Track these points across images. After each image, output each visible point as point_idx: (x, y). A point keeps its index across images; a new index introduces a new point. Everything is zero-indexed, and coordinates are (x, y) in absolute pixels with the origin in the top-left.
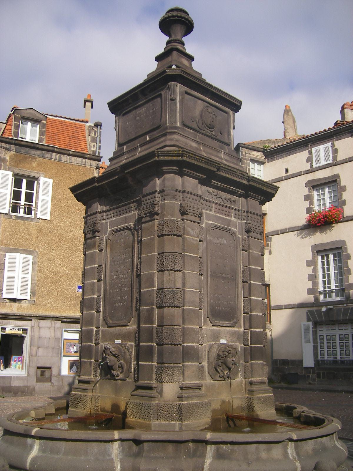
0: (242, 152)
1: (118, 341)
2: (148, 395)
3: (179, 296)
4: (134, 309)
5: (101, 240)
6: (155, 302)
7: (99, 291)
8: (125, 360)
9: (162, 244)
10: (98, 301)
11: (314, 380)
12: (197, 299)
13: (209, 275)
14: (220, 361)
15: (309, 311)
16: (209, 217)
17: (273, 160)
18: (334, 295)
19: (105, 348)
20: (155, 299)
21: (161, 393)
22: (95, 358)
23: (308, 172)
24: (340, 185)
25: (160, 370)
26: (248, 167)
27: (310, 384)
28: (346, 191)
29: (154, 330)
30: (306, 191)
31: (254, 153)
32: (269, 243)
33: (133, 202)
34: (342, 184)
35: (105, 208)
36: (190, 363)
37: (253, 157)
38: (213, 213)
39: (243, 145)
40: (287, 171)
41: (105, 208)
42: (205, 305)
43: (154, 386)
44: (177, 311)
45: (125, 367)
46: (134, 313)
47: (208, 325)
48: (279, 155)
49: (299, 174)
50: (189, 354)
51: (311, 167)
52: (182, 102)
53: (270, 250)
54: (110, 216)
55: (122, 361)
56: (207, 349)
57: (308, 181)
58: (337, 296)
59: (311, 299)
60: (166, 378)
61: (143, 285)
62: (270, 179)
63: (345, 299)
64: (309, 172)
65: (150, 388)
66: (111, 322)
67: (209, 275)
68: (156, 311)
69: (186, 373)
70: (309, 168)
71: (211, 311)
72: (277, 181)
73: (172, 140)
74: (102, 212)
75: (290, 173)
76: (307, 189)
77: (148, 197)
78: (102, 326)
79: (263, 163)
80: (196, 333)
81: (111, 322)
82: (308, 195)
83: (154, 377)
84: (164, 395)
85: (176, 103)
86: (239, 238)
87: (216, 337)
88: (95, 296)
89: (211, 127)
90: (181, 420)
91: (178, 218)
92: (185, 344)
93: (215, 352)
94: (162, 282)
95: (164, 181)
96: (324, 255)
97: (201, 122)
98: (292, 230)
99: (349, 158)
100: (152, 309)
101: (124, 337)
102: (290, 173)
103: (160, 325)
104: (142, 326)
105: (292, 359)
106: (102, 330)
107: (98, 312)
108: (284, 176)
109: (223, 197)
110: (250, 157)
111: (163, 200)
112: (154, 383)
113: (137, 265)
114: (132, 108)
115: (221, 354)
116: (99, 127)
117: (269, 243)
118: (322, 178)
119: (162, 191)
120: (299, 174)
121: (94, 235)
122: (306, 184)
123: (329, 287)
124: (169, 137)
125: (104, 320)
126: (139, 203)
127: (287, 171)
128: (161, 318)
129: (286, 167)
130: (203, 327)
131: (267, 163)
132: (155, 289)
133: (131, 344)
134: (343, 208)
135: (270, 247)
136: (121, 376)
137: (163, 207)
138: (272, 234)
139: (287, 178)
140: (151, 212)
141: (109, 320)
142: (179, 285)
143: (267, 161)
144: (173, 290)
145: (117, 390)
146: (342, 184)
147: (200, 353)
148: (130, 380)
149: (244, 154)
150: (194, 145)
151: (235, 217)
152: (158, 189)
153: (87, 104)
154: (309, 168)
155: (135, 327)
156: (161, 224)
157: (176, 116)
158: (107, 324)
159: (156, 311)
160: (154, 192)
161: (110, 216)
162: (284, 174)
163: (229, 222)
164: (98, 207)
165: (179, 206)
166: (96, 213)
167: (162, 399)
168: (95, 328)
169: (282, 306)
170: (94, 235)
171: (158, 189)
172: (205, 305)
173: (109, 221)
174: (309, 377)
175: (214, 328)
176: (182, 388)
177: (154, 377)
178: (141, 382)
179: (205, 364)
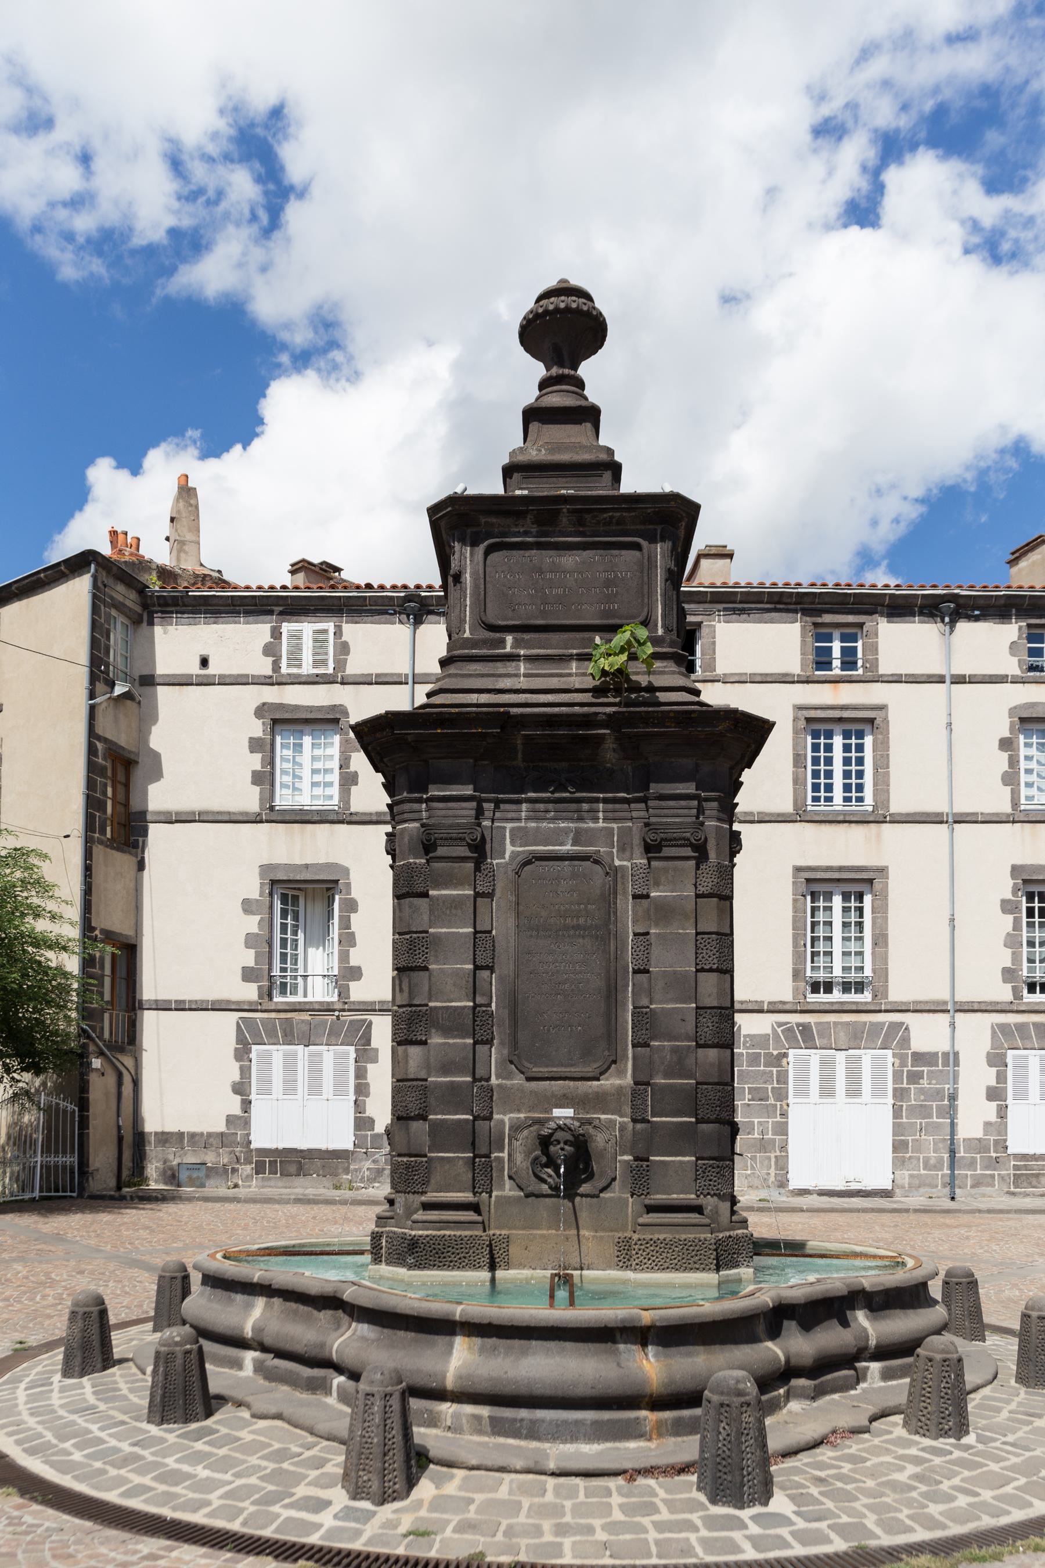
11: (249, 1178)
30: (258, 729)
32: (141, 839)
40: (204, 662)
57: (264, 704)
59: (250, 992)
72: (176, 681)
75: (213, 670)
102: (213, 670)
108: (197, 676)
117: (141, 839)
127: (204, 662)
129: (204, 653)
162: (195, 669)
175: (534, 1084)
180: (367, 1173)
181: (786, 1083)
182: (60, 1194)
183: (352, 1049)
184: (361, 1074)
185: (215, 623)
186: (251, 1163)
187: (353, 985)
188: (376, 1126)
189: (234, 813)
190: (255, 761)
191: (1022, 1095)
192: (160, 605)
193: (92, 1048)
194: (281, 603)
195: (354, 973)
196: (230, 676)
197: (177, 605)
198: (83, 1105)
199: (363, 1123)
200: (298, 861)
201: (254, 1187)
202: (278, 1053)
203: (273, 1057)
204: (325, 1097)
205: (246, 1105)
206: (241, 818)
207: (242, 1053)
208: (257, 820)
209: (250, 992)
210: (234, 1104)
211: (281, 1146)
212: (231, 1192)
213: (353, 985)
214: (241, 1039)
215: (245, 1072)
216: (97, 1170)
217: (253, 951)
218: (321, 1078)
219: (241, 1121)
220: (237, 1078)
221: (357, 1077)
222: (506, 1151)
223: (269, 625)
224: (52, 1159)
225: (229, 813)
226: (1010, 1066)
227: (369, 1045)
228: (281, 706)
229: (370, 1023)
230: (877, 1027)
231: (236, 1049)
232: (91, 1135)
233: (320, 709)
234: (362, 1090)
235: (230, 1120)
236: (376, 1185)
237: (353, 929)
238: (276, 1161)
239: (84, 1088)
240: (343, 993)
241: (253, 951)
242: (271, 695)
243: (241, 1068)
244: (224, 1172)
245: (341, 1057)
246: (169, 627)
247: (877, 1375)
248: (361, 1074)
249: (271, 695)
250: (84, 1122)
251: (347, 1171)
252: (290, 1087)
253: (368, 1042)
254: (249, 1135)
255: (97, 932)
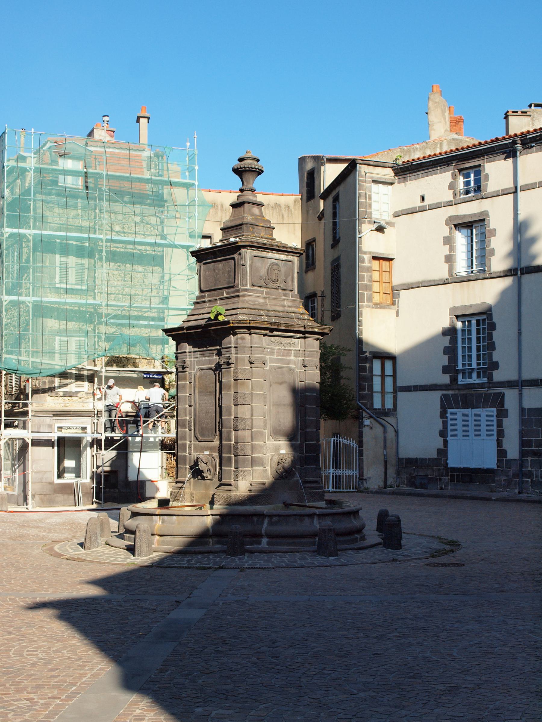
0: (360, 171)
1: (207, 453)
2: (229, 489)
3: (248, 422)
4: (218, 430)
5: (190, 374)
6: (232, 427)
7: (190, 414)
8: (212, 465)
9: (236, 385)
10: (190, 422)
11: (446, 484)
12: (262, 424)
13: (271, 405)
14: (279, 466)
15: (443, 395)
16: (271, 361)
17: (405, 179)
18: (474, 375)
19: (197, 458)
20: (232, 425)
21: (237, 488)
22: (189, 464)
23: (449, 204)
24: (489, 227)
25: (236, 472)
26: (368, 193)
27: (441, 489)
28: (495, 236)
29: (232, 446)
30: (445, 231)
31: (379, 170)
32: (397, 300)
33: (215, 350)
34: (492, 226)
35: (192, 350)
36: (257, 468)
37: (376, 177)
38: (275, 357)
39: (361, 162)
40: (423, 198)
41: (192, 350)
42: (268, 426)
43: (232, 483)
44: (247, 433)
45: (212, 471)
46: (218, 433)
47: (271, 441)
48: (414, 174)
49: (437, 206)
50: (254, 462)
51: (454, 197)
52: (251, 265)
53: (398, 310)
54: (196, 356)
55: (210, 467)
56: (270, 458)
57: (450, 217)
58: (479, 376)
59: (446, 379)
60: (240, 478)
61: (223, 414)
62: (401, 209)
63: (487, 381)
64: (450, 204)
65: (230, 485)
66: (200, 438)
67: (271, 405)
68: (233, 433)
69: (254, 474)
70: (451, 198)
71: (273, 431)
73: (243, 301)
74: (190, 352)
75: (426, 203)
76: (447, 228)
77: (226, 350)
78: (194, 441)
79: (392, 184)
80: (261, 447)
81: (200, 438)
82: (448, 237)
83: (233, 477)
84: (239, 489)
85: (246, 268)
86: (297, 372)
87: (277, 449)
88: (188, 418)
89: (275, 281)
90: (55, 353)
91: (248, 367)
92: (253, 455)
93: (276, 459)
94: (237, 413)
95: (237, 339)
96: (465, 321)
97: (267, 278)
98: (426, 285)
99: (502, 190)
100: (231, 431)
101: (211, 449)
102: (426, 203)
103: (236, 443)
104: (224, 442)
105: (422, 457)
106: (194, 444)
107: (190, 430)
109: (283, 343)
110: (372, 177)
111: (237, 353)
112: (232, 481)
113: (219, 398)
114: (210, 260)
115: (280, 461)
116: (160, 158)
118: (467, 215)
119: (235, 347)
120: (437, 206)
121: (184, 370)
122: (447, 220)
123: (470, 365)
124: (241, 298)
125: (195, 436)
126: (219, 354)
127: (423, 198)
128: (236, 438)
129: (422, 194)
130: (267, 443)
131: (396, 184)
132: (233, 417)
133: (216, 455)
134: (490, 260)
135: (398, 306)
136: (209, 477)
137: (237, 358)
138: (400, 288)
139: (422, 210)
140: (228, 362)
141: (199, 436)
142: (248, 414)
143: (397, 181)
144: (244, 419)
145: (207, 488)
146: (492, 226)
147: (264, 461)
148: (216, 480)
149: (363, 174)
150: (261, 301)
151: (294, 356)
152: (233, 345)
153: (141, 119)
154: (451, 198)
155: (218, 442)
156: (236, 371)
157: (246, 279)
158: (197, 439)
159: (233, 433)
160: (230, 347)
161: (196, 356)
162: (418, 203)
163: (289, 362)
164: (188, 348)
165: (248, 358)
166: (185, 352)
167: (238, 492)
168: (188, 443)
169: (410, 386)
170: (184, 370)
171: (233, 345)
172: (268, 426)
173: (196, 359)
174: (441, 479)
176: (251, 484)
177: (233, 477)
178: (224, 481)
179: (268, 468)
180: (503, 483)
181: (447, 428)
182: (352, 490)
183: (495, 410)
184: (500, 424)
185: (427, 176)
186: (448, 476)
187: (495, 373)
188: (508, 455)
189: (436, 280)
190: (446, 250)
191: (455, 435)
192: (402, 172)
193: (364, 414)
194: (454, 158)
195: (495, 366)
196: (433, 204)
197: (409, 170)
198: (361, 444)
199: (502, 453)
200: (467, 304)
201: (450, 490)
202: (459, 412)
203: (457, 414)
204: (482, 438)
205: (446, 442)
206: (439, 283)
207: (443, 415)
208: (445, 283)
209: (446, 379)
210: (439, 443)
211: (462, 466)
212: (440, 492)
213: (495, 373)
214: (442, 406)
215: (445, 424)
216: (369, 478)
217: (447, 356)
218: (480, 426)
219: (443, 452)
220: (441, 428)
221: (498, 427)
222: (233, 465)
223: (451, 172)
224: (338, 472)
225: (434, 281)
226: (449, 418)
227: (503, 407)
228: (457, 217)
229: (504, 394)
230: (488, 396)
231: (441, 411)
232: (364, 460)
233: (475, 215)
234: (501, 433)
235: (439, 451)
236: (508, 489)
237: (494, 340)
238: (459, 475)
239: (361, 435)
240: (490, 378)
241: (447, 356)
242: (452, 211)
243: (443, 422)
244: (436, 480)
245: (489, 414)
246: (407, 183)
247: (265, 543)
248: (500, 424)
249: (452, 211)
250: (361, 454)
251: (493, 481)
252: (466, 433)
253: (503, 405)
254: (447, 460)
255: (367, 354)
